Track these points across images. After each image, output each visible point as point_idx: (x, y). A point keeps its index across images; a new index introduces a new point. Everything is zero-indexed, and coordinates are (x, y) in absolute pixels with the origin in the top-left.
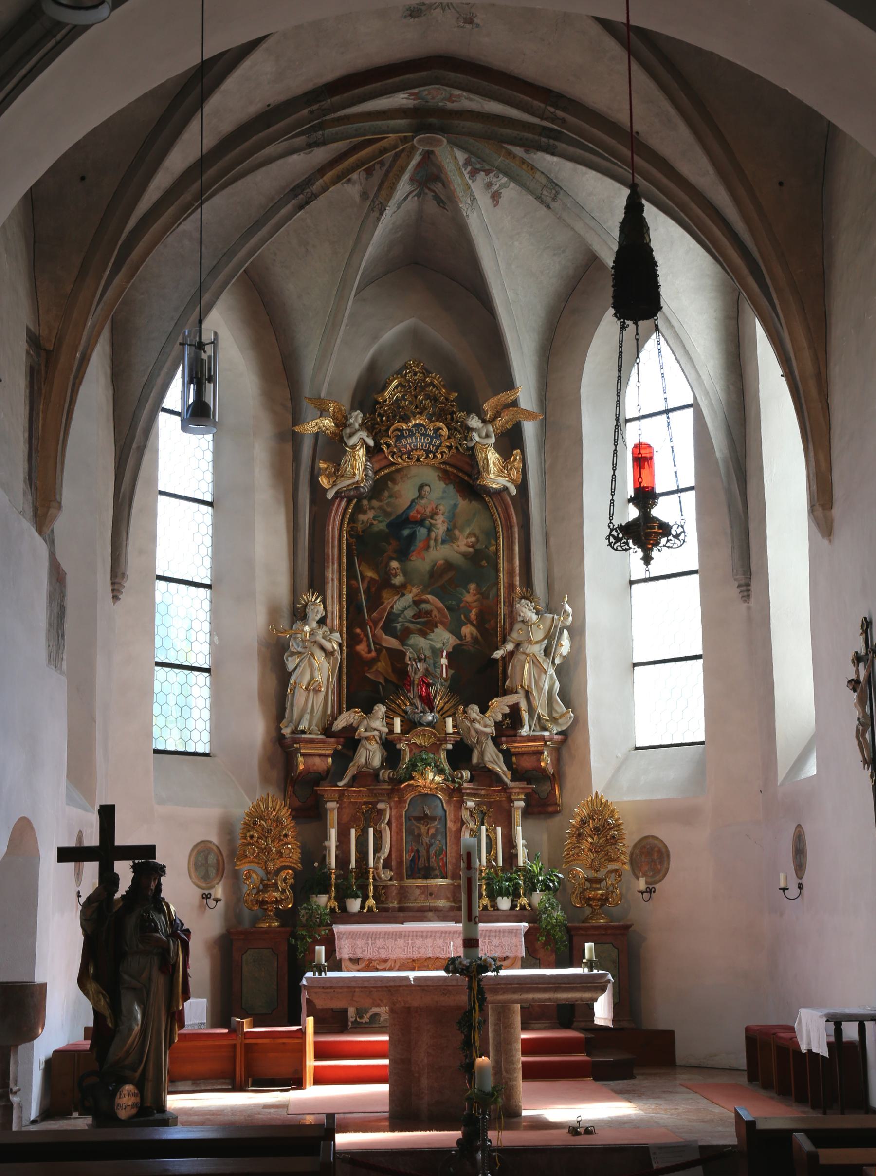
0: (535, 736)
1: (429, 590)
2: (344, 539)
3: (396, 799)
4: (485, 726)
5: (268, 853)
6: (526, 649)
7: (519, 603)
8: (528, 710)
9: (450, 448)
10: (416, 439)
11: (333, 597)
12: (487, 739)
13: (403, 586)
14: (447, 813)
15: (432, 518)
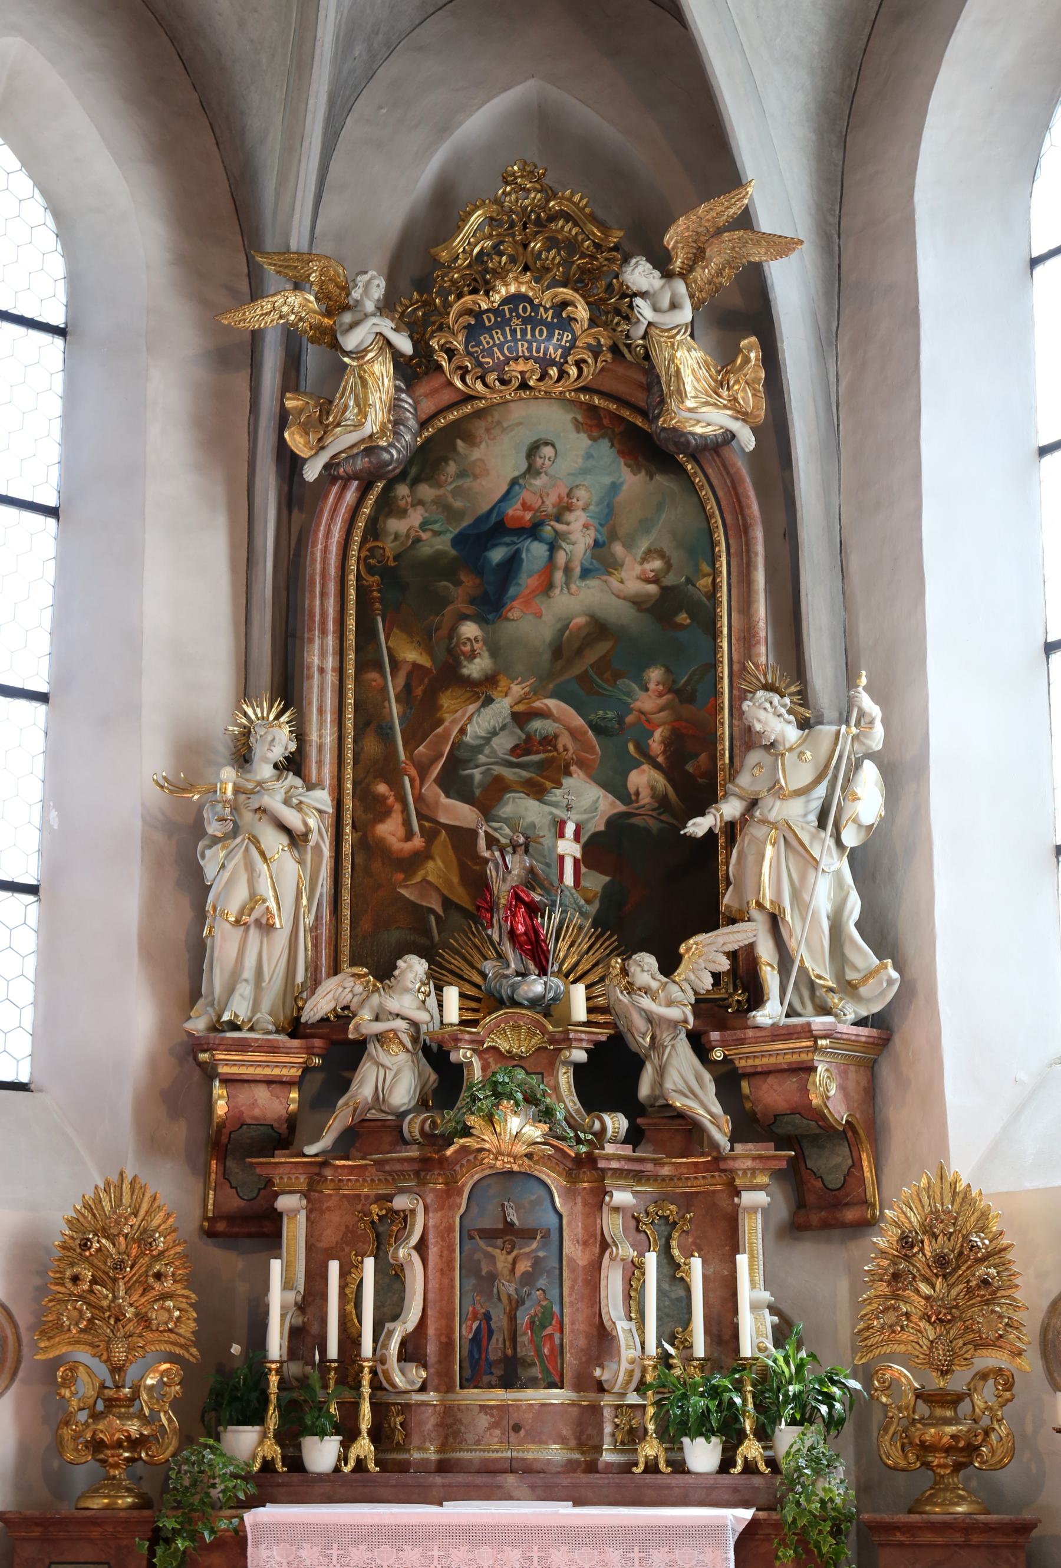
0: (789, 1026)
1: (551, 686)
2: (352, 578)
3: (439, 1187)
4: (670, 1003)
5: (117, 1320)
6: (770, 811)
9: (596, 353)
10: (513, 332)
11: (321, 711)
12: (674, 1038)
13: (490, 680)
14: (564, 1222)
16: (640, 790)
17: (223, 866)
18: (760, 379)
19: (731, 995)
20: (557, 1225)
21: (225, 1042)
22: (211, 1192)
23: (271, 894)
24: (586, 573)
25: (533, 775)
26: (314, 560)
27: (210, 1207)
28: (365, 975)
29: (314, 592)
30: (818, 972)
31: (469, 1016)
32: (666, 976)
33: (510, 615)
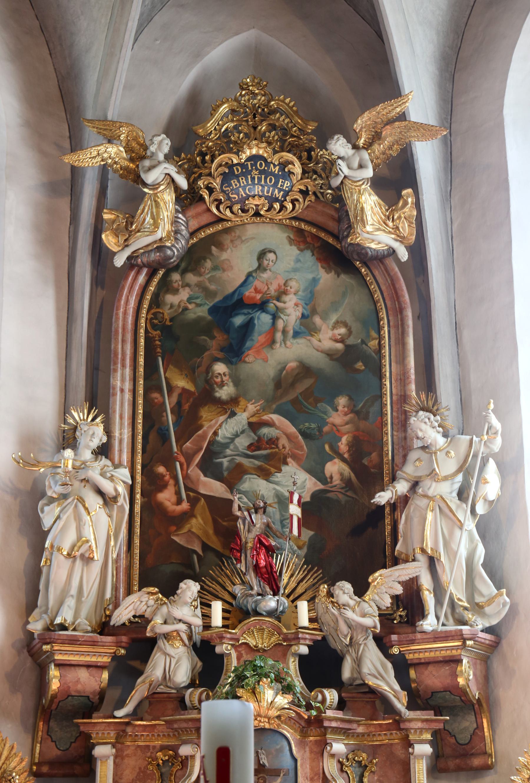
1: (274, 406)
2: (142, 331)
4: (364, 615)
6: (429, 489)
7: (415, 416)
8: (434, 591)
9: (305, 193)
10: (253, 179)
11: (121, 417)
12: (366, 639)
13: (234, 401)
15: (278, 299)
16: (333, 475)
17: (58, 518)
18: (413, 216)
19: (395, 612)
20: (293, 766)
21: (61, 638)
22: (38, 745)
23: (92, 537)
24: (296, 334)
25: (263, 463)
26: (117, 318)
27: (37, 755)
28: (155, 594)
29: (118, 339)
30: (458, 596)
31: (227, 623)
32: (359, 597)
33: (247, 359)
